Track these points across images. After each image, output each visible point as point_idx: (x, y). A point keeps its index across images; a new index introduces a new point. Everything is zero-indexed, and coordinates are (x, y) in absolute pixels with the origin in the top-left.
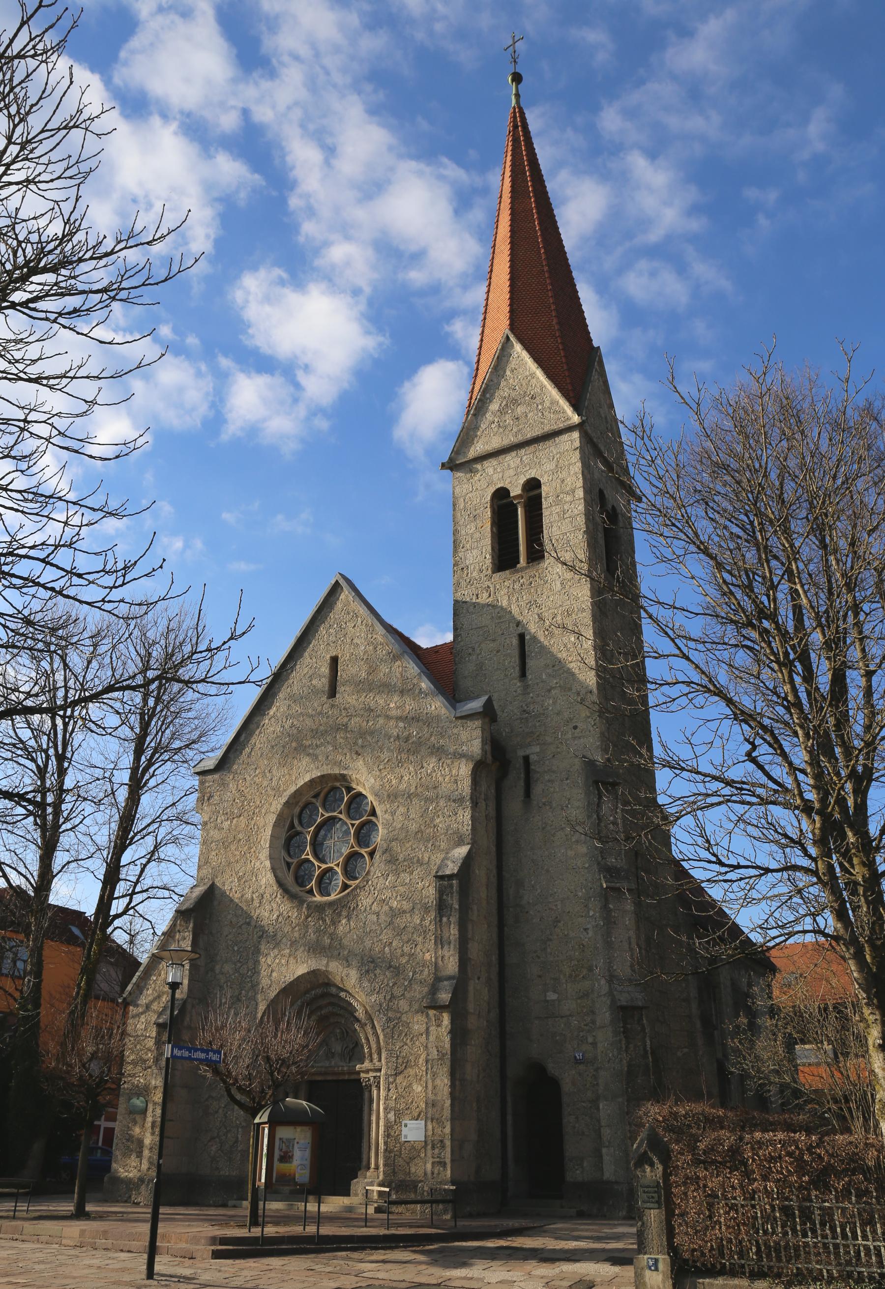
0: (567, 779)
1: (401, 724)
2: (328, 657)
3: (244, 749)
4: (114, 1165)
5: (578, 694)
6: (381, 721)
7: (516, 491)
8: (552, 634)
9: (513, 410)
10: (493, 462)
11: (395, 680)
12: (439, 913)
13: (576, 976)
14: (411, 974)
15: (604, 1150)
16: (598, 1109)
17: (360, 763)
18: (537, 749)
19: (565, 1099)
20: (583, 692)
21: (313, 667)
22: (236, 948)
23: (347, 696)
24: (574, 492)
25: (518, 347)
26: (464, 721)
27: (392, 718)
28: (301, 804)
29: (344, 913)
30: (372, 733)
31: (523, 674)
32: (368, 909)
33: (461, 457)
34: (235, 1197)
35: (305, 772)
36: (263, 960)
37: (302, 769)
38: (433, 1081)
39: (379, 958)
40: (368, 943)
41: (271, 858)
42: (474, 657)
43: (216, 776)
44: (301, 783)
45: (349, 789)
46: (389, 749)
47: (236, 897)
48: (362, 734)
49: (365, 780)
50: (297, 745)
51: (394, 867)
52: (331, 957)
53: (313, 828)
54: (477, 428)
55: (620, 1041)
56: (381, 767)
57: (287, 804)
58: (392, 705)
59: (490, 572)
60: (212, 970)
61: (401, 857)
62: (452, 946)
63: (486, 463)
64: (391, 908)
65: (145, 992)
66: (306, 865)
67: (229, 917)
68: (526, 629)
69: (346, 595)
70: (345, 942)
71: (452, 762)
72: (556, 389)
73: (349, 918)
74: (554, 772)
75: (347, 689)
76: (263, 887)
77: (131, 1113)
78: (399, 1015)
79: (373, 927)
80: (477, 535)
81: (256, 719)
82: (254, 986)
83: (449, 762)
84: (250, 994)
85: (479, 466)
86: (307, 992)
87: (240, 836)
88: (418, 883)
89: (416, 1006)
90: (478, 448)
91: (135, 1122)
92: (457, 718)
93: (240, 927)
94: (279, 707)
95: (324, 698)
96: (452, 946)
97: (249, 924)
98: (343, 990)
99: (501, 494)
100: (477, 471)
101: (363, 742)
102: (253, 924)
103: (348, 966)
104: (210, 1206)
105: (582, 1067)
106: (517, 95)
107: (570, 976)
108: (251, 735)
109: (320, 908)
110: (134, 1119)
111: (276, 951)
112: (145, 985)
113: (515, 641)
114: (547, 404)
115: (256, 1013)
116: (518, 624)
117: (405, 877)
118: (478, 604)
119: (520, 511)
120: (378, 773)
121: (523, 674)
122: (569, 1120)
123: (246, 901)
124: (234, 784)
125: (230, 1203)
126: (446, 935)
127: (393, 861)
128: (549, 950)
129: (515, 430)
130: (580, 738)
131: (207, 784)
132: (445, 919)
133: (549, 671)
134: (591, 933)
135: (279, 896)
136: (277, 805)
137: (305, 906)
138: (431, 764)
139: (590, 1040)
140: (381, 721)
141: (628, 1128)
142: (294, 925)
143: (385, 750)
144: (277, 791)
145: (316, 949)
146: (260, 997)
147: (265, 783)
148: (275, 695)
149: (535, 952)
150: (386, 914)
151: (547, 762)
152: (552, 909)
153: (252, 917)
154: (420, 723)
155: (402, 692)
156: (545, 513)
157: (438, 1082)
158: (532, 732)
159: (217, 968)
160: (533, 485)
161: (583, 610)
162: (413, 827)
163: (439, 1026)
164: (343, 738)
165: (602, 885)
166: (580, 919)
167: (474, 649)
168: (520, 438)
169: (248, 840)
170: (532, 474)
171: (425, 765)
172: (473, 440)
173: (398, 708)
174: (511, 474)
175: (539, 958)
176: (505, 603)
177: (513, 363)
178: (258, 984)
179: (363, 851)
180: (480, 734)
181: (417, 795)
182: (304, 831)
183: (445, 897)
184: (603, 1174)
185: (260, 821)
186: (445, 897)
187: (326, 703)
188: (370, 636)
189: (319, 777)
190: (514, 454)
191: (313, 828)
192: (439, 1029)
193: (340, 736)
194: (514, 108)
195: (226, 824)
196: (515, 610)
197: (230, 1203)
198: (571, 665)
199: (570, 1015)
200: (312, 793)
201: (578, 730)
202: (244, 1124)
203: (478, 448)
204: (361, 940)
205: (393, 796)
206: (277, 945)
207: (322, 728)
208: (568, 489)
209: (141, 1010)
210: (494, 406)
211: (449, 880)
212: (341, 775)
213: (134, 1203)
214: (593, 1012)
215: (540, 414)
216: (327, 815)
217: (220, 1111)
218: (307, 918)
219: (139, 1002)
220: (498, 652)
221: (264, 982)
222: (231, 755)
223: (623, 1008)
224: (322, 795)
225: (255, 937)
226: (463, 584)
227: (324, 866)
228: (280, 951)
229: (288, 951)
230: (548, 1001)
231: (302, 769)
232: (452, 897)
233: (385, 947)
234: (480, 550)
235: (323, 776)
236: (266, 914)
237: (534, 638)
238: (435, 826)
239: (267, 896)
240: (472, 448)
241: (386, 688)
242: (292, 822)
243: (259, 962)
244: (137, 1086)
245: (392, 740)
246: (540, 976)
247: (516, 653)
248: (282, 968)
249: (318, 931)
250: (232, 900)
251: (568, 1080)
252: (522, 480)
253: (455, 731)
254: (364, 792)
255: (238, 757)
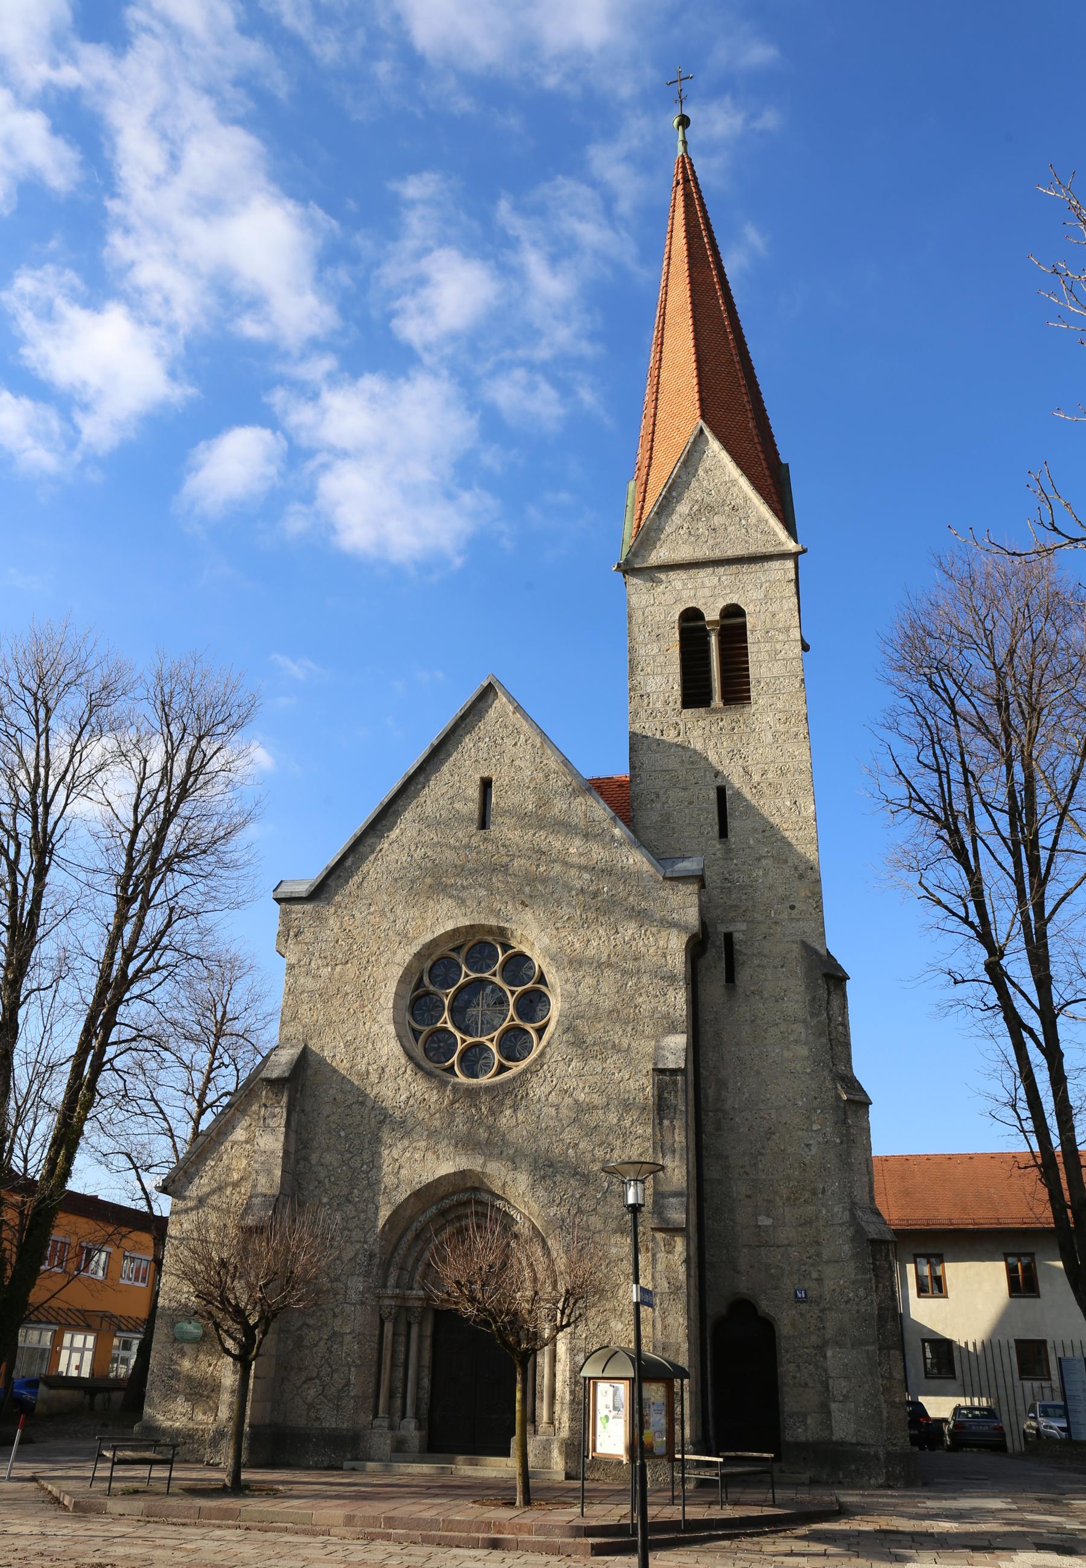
0: (782, 967)
1: (586, 876)
2: (477, 777)
3: (351, 877)
4: (148, 1410)
5: (796, 869)
6: (558, 868)
7: (712, 614)
8: (761, 794)
9: (708, 519)
10: (683, 575)
11: (577, 819)
12: (659, 1114)
13: (796, 1199)
14: (606, 1184)
15: (834, 1406)
16: (825, 1357)
17: (528, 916)
18: (743, 926)
19: (783, 1344)
20: (802, 867)
21: (453, 788)
22: (343, 1134)
23: (503, 829)
24: (788, 631)
25: (714, 446)
26: (674, 883)
27: (572, 866)
28: (434, 957)
29: (508, 1102)
30: (544, 881)
31: (723, 833)
32: (543, 1099)
33: (638, 560)
34: (349, 1456)
35: (445, 918)
36: (386, 1152)
37: (441, 913)
38: (663, 1320)
39: (561, 1162)
40: (543, 1143)
41: (396, 1022)
42: (659, 805)
43: (308, 907)
44: (440, 931)
45: (506, 947)
46: (569, 904)
47: (343, 1067)
48: (531, 880)
49: (534, 937)
50: (433, 881)
51: (579, 1051)
52: (489, 1157)
53: (452, 990)
54: (660, 530)
55: (871, 1279)
56: (559, 925)
57: (418, 955)
58: (571, 850)
59: (679, 705)
60: (306, 1159)
61: (589, 1040)
62: (677, 1156)
63: (672, 575)
64: (576, 1101)
65: (196, 1181)
66: (441, 1036)
67: (331, 1092)
68: (729, 782)
69: (501, 702)
70: (511, 1137)
71: (659, 932)
72: (766, 506)
73: (515, 1108)
74: (765, 956)
75: (507, 821)
76: (384, 1058)
77: (175, 1340)
78: (589, 1234)
79: (551, 1123)
80: (661, 659)
81: (370, 841)
82: (373, 1185)
83: (654, 930)
84: (366, 1195)
85: (663, 576)
86: (443, 1198)
87: (348, 989)
88: (614, 1074)
89: (613, 1225)
90: (660, 554)
91: (183, 1355)
92: (665, 878)
93: (349, 1107)
94: (405, 828)
95: (473, 828)
96: (677, 1156)
97: (362, 1104)
98: (499, 1197)
99: (691, 617)
100: (661, 581)
101: (533, 890)
102: (369, 1104)
103: (515, 1169)
104: (309, 1468)
105: (804, 1307)
106: (685, 142)
107: (788, 1199)
108: (363, 859)
109: (472, 1094)
110: (182, 1349)
111: (406, 1142)
112: (198, 1171)
113: (713, 795)
114: (753, 520)
115: (376, 1219)
116: (717, 774)
117: (596, 1065)
118: (663, 741)
119: (714, 640)
120: (554, 932)
121: (723, 833)
122: (787, 1369)
123: (359, 1074)
124: (334, 921)
125: (347, 1464)
126: (668, 1141)
127: (578, 1042)
128: (760, 1166)
129: (711, 542)
130: (798, 920)
131: (294, 916)
132: (666, 1122)
133: (759, 836)
134: (814, 1151)
135: (409, 1071)
136: (405, 955)
137: (450, 1087)
138: (630, 929)
139: (815, 1275)
140: (558, 868)
141: (880, 1381)
142: (432, 1111)
143: (564, 904)
144: (405, 938)
145: (467, 1143)
146: (382, 1200)
147: (385, 925)
148: (398, 814)
149: (743, 1167)
150: (569, 1108)
151: (756, 944)
152: (765, 1118)
153: (367, 1095)
154: (613, 878)
155: (586, 836)
156: (751, 648)
157: (670, 1320)
158: (736, 906)
159: (314, 1158)
160: (733, 612)
161: (801, 772)
162: (607, 1004)
163: (669, 1252)
164: (503, 882)
165: (838, 1097)
166: (800, 1133)
167: (658, 796)
168: (717, 554)
169: (360, 996)
170: (734, 599)
171: (620, 929)
172: (655, 543)
173: (581, 855)
174: (710, 595)
175: (747, 1174)
176: (699, 746)
177: (707, 462)
178: (379, 1182)
179: (528, 1027)
180: (697, 901)
181: (610, 965)
182: (440, 992)
183: (666, 1095)
184: (832, 1433)
185: (379, 973)
186: (666, 1095)
187: (475, 834)
188: (538, 760)
189: (466, 927)
190: (710, 570)
191: (452, 990)
192: (670, 1256)
193: (497, 881)
194: (682, 156)
195: (325, 971)
196: (712, 757)
197: (347, 1464)
198: (787, 834)
199: (789, 1245)
200: (451, 946)
201: (796, 911)
202: (358, 1362)
203: (660, 554)
204: (533, 1137)
205: (576, 963)
206: (408, 1134)
207: (470, 865)
208: (780, 626)
209: (190, 1204)
210: (683, 508)
211: (671, 1075)
212: (499, 928)
213: (208, 1464)
214: (818, 1243)
215: (743, 531)
216: (473, 975)
217: (322, 1343)
218: (453, 1103)
219: (187, 1193)
220: (690, 803)
221: (388, 1180)
222: (331, 882)
223: (873, 1242)
224: (466, 949)
225: (372, 1124)
226: (643, 715)
227: (470, 1040)
228: (411, 1143)
229: (424, 1143)
230: (759, 1227)
231: (441, 913)
232: (676, 1097)
233: (568, 1149)
234: (664, 677)
235: (472, 926)
236: (390, 1094)
237: (738, 794)
238: (636, 1007)
239: (390, 1070)
240: (654, 553)
241: (563, 826)
242: (421, 979)
243: (380, 1154)
244: (186, 1305)
245: (574, 893)
246: (749, 1197)
247: (714, 807)
248: (414, 1166)
249: (470, 1120)
250: (335, 1071)
251: (786, 1321)
252: (721, 604)
253: (662, 894)
254: (528, 953)
255: (342, 886)
